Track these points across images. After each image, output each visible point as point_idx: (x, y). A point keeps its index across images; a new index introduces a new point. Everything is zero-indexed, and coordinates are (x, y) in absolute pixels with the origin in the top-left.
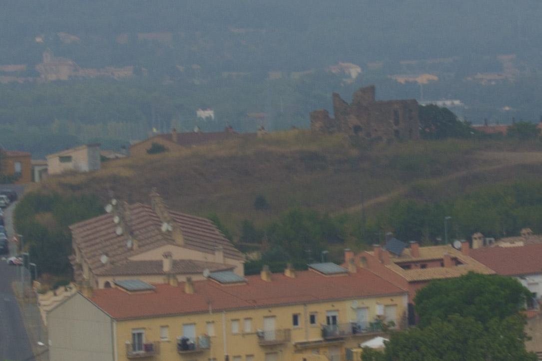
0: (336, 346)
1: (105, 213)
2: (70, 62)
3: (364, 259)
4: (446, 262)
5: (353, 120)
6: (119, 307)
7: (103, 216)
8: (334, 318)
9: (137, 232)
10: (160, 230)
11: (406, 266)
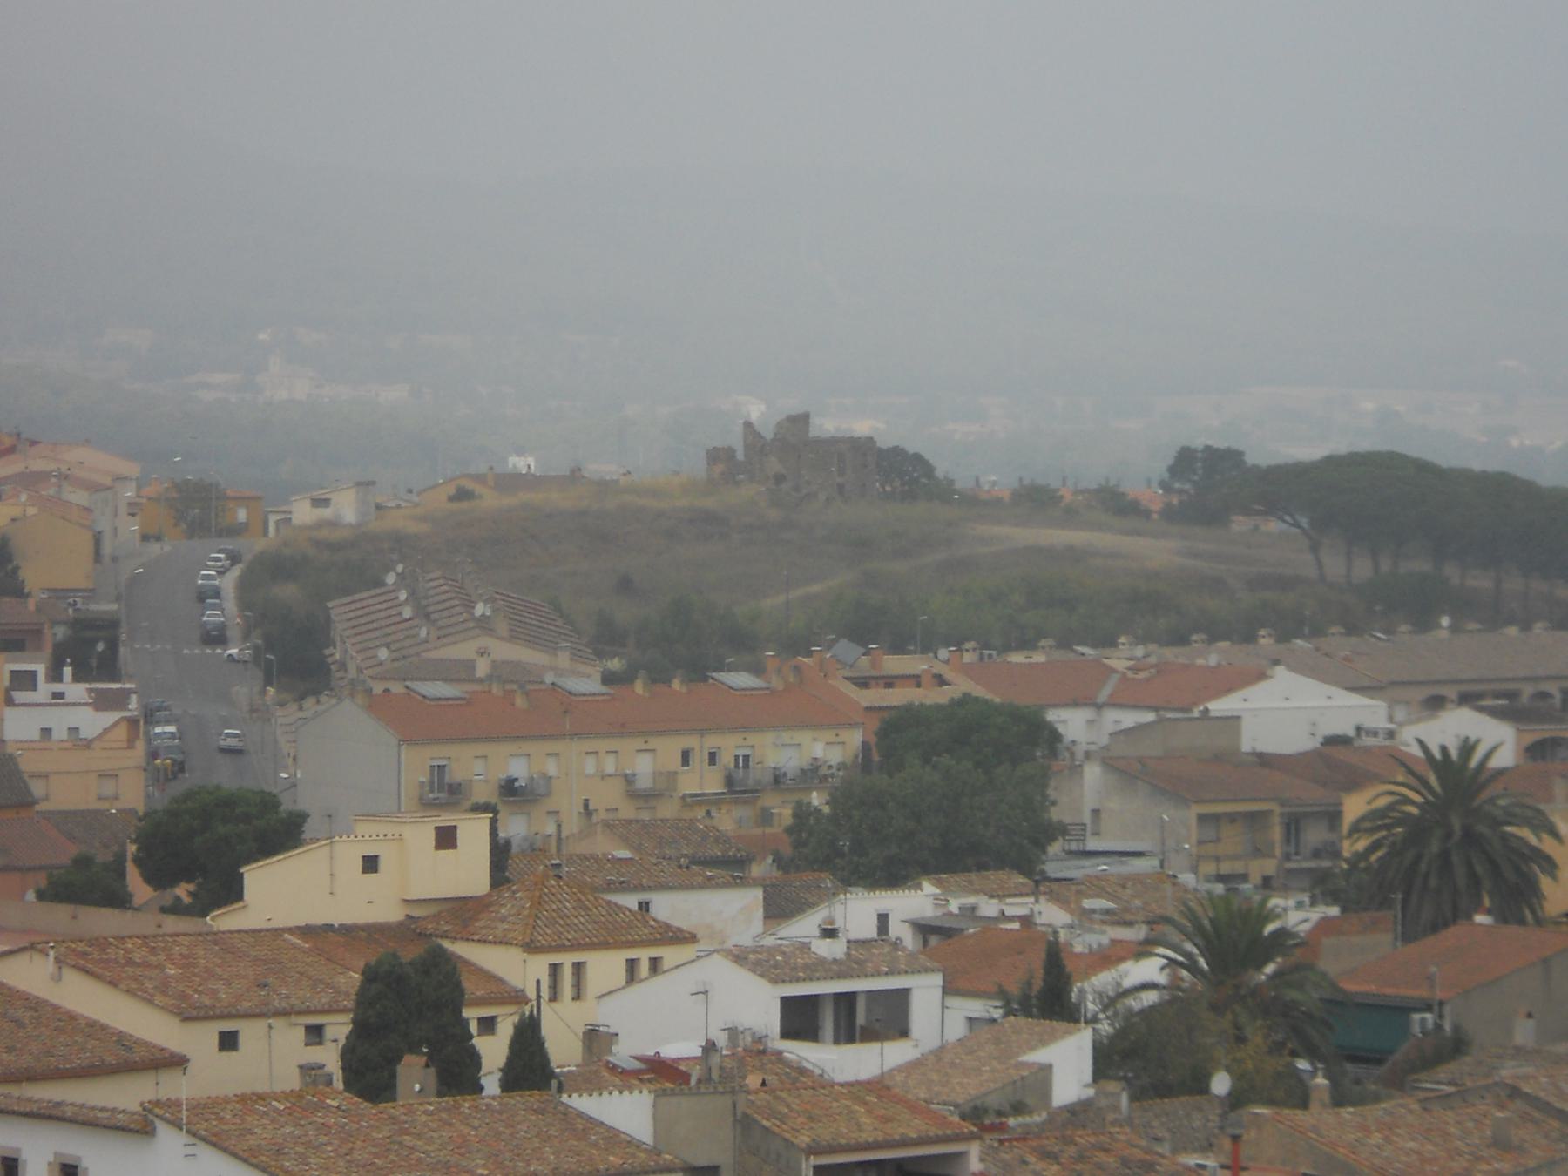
0: (745, 802)
1: (383, 584)
5: (774, 465)
6: (415, 723)
8: (746, 758)
11: (863, 683)
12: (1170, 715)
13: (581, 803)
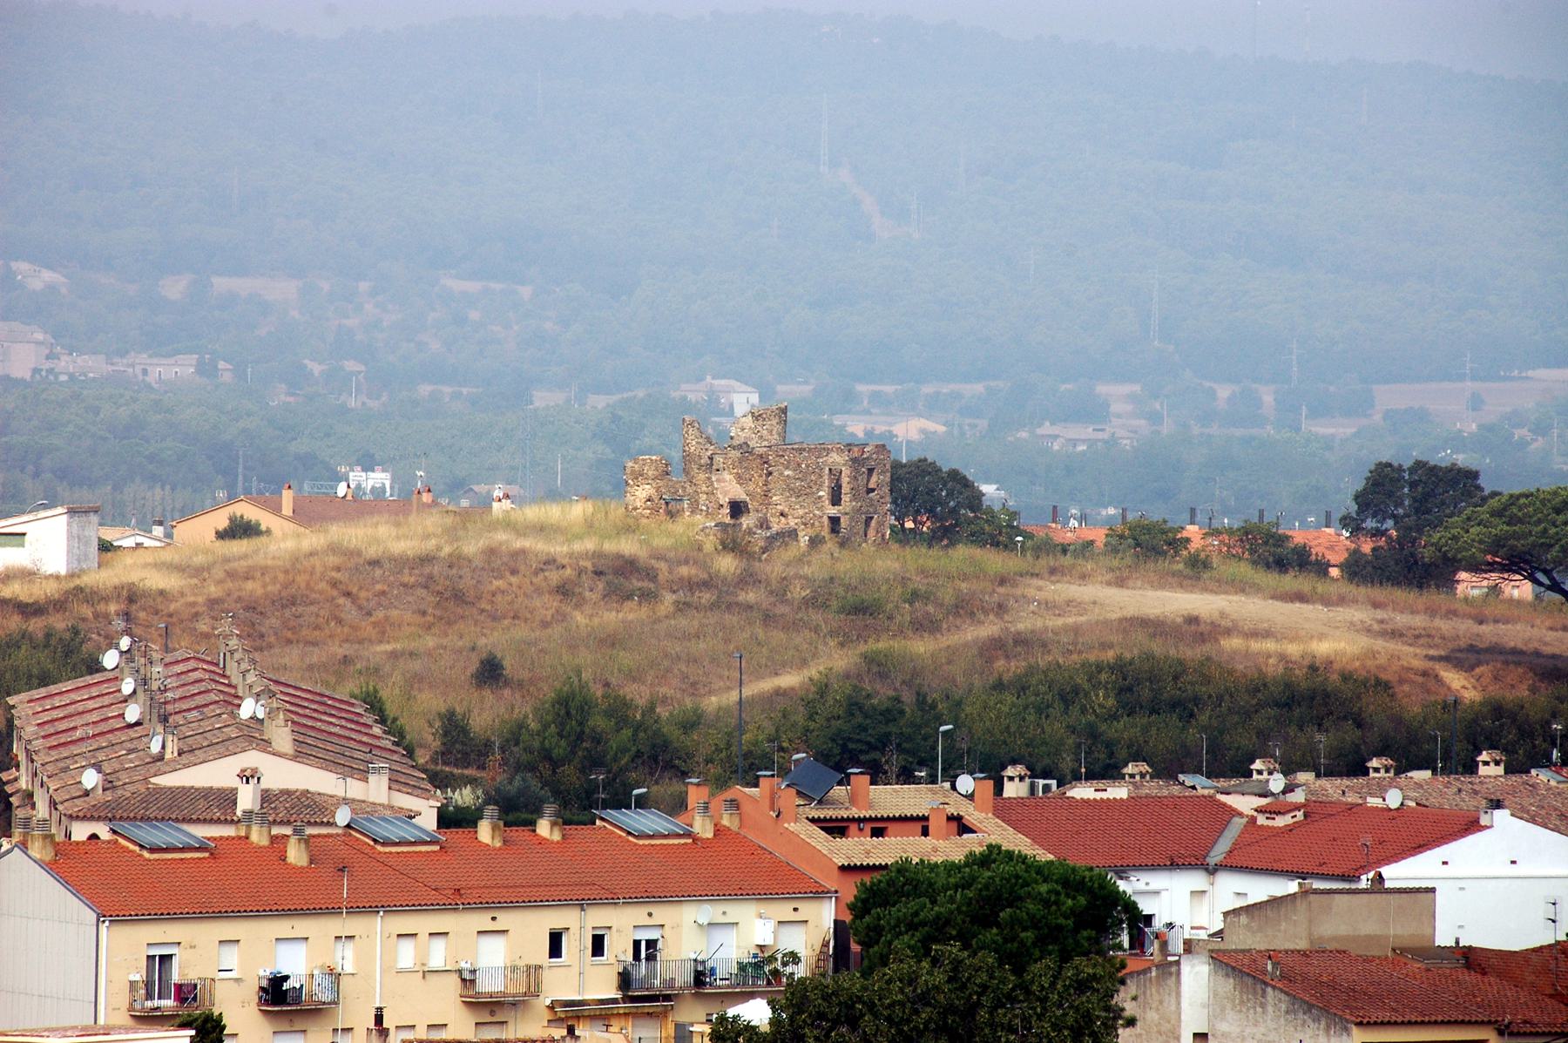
2: (39, 336)
3: (734, 804)
4: (936, 824)
7: (98, 677)
9: (179, 719)
10: (234, 715)
11: (836, 828)
12: (1318, 885)
13: (373, 1012)
